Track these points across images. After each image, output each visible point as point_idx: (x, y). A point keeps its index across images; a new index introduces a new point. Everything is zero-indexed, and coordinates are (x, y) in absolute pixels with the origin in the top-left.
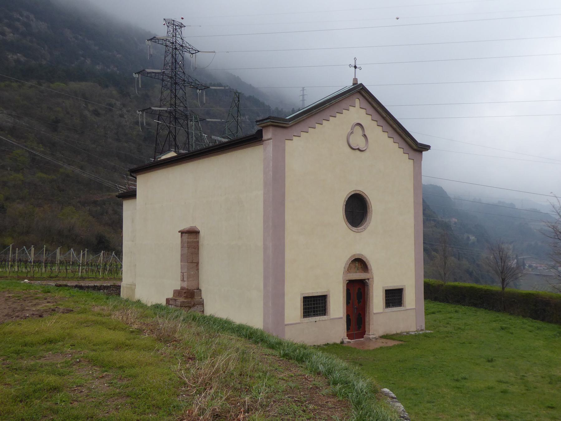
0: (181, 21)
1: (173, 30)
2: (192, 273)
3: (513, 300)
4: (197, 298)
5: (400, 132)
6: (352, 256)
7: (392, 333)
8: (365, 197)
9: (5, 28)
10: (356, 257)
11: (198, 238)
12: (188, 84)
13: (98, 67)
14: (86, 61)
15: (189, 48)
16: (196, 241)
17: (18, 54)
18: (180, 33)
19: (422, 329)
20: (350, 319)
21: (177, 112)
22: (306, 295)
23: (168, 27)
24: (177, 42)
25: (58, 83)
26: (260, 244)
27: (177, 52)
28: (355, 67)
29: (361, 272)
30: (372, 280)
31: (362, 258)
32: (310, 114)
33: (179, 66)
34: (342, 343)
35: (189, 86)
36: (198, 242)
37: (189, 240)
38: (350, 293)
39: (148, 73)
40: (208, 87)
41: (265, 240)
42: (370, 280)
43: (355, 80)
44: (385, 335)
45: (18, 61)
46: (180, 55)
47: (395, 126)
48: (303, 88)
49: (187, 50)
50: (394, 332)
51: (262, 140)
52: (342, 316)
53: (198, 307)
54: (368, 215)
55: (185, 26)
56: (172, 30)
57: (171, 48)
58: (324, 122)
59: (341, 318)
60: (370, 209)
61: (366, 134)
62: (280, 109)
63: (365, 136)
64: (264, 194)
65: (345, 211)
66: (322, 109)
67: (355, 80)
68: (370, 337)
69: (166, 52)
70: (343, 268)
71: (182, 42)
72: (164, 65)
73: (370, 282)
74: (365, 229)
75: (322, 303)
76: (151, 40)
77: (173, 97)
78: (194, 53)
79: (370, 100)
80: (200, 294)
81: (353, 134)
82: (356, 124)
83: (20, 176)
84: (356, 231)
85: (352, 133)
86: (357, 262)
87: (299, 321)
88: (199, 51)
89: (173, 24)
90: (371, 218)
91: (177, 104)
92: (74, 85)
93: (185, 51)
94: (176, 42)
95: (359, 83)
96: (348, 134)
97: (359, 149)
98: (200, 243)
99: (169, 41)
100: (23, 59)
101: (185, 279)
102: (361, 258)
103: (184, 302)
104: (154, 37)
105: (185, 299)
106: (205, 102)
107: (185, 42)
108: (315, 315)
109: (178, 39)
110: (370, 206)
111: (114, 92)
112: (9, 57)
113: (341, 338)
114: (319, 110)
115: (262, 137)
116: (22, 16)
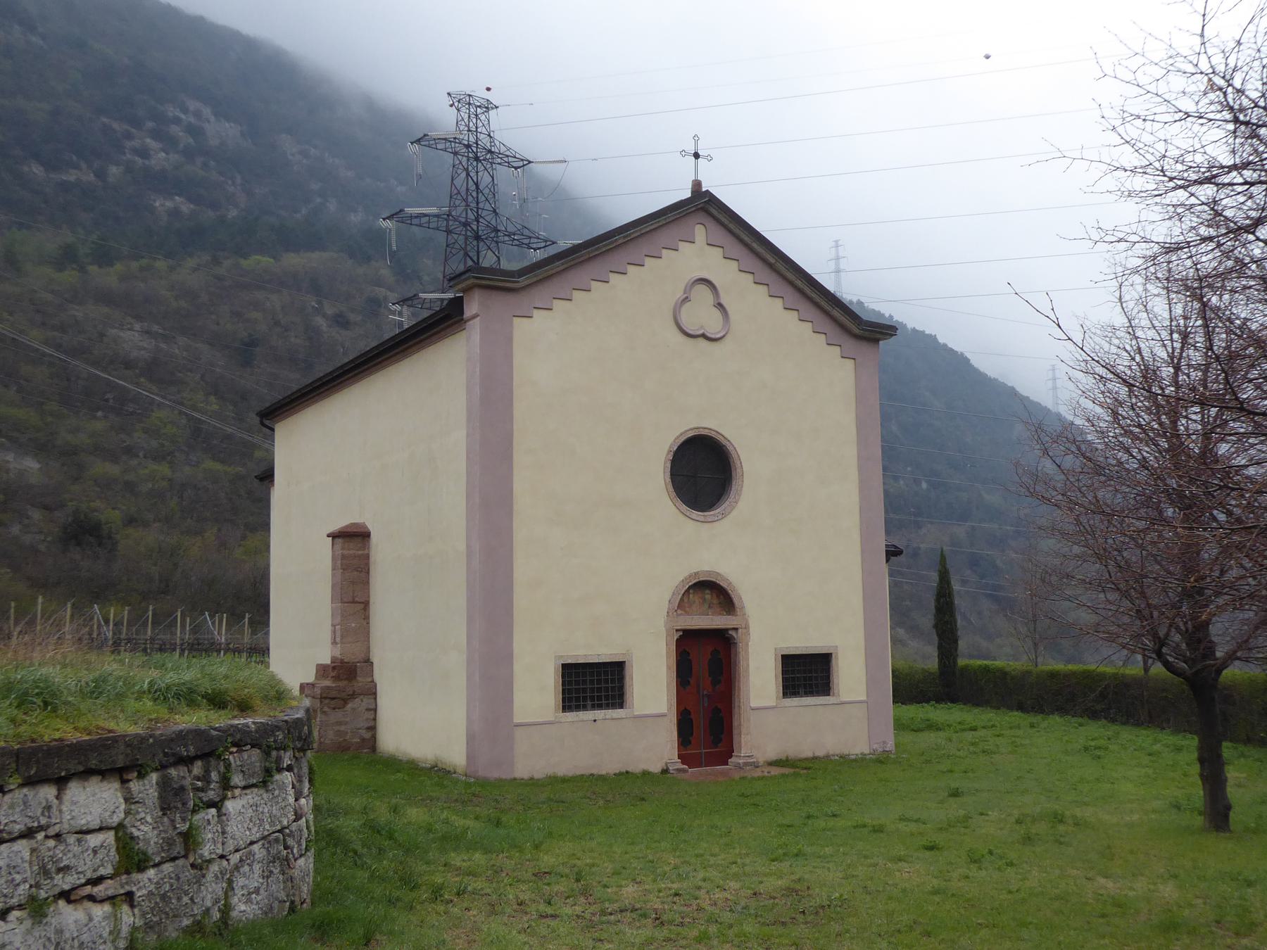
0: (487, 95)
1: (469, 117)
2: (353, 625)
3: (1164, 694)
4: (361, 680)
5: (813, 295)
7: (804, 755)
9: (148, 140)
10: (701, 579)
11: (369, 548)
12: (507, 238)
13: (356, 218)
14: (328, 204)
15: (508, 156)
16: (362, 555)
17: (177, 198)
18: (486, 123)
19: (888, 749)
20: (692, 720)
22: (570, 661)
23: (458, 110)
24: (479, 143)
25: (257, 257)
26: (462, 547)
28: (696, 156)
29: (720, 614)
30: (744, 631)
32: (573, 259)
33: (484, 199)
34: (665, 771)
36: (367, 557)
37: (346, 552)
38: (690, 660)
39: (411, 217)
40: (554, 243)
41: (468, 538)
43: (697, 185)
44: (784, 758)
45: (175, 213)
47: (799, 283)
48: (836, 242)
50: (808, 754)
51: (462, 319)
53: (362, 701)
54: (734, 483)
55: (497, 107)
56: (467, 116)
57: (465, 159)
59: (663, 715)
60: (738, 470)
61: (723, 302)
63: (720, 306)
64: (468, 436)
65: (671, 475)
67: (697, 185)
68: (741, 761)
70: (667, 602)
71: (491, 142)
72: (451, 197)
74: (724, 515)
75: (613, 681)
76: (418, 141)
78: (519, 167)
79: (731, 226)
80: (371, 673)
81: (688, 304)
83: (164, 469)
84: (702, 519)
86: (708, 591)
88: (530, 162)
89: (469, 104)
90: (741, 490)
92: (294, 261)
93: (499, 164)
94: (477, 144)
96: (676, 304)
97: (704, 336)
98: (372, 559)
99: (460, 143)
100: (186, 208)
101: (338, 640)
103: (328, 687)
104: (425, 135)
105: (334, 682)
107: (497, 143)
108: (600, 707)
110: (738, 463)
111: (385, 272)
112: (157, 204)
113: (664, 761)
115: (462, 313)
116: (185, 110)
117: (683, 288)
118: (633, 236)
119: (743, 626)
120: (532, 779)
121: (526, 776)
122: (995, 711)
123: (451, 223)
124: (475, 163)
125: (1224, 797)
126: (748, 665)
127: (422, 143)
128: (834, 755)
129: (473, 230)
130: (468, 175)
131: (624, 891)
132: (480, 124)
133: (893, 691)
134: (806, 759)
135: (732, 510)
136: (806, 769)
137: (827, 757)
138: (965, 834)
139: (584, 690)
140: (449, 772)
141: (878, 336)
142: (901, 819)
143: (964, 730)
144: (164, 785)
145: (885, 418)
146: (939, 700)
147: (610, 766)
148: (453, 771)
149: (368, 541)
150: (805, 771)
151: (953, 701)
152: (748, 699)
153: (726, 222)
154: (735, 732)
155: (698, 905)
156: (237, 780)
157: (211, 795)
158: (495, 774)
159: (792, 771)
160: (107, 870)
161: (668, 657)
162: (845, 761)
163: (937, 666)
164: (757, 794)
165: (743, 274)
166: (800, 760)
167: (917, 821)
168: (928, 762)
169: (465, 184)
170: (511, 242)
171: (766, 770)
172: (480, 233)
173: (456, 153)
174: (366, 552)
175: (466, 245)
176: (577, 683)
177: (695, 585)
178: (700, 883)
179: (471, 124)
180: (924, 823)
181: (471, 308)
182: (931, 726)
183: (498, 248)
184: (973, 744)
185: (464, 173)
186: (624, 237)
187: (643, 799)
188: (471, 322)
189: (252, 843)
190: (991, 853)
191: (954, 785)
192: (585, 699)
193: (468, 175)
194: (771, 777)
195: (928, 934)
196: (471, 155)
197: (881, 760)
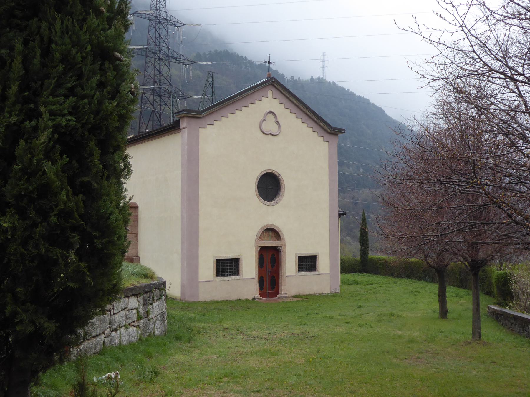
1: (157, 3)
7: (305, 294)
8: (278, 175)
15: (174, 22)
18: (164, 6)
21: (161, 90)
26: (179, 215)
27: (161, 27)
29: (275, 241)
34: (254, 299)
35: (175, 62)
41: (182, 212)
42: (282, 247)
46: (164, 29)
48: (324, 53)
49: (171, 24)
54: (281, 191)
57: (155, 23)
58: (237, 112)
60: (283, 186)
62: (296, 78)
64: (182, 173)
66: (234, 101)
69: (149, 26)
71: (166, 15)
72: (148, 40)
74: (277, 203)
77: (157, 74)
78: (179, 27)
82: (268, 113)
84: (269, 204)
85: (264, 120)
86: (270, 232)
87: (212, 279)
88: (184, 25)
91: (161, 81)
93: (170, 25)
95: (271, 76)
97: (271, 134)
98: (139, 217)
104: (136, 12)
106: (191, 78)
108: (230, 275)
109: (162, 12)
113: (254, 295)
114: (231, 101)
115: (180, 126)
117: (263, 116)
118: (244, 96)
120: (205, 302)
121: (203, 300)
122: (382, 277)
123: (148, 52)
124: (159, 25)
125: (446, 308)
127: (135, 15)
128: (317, 294)
129: (158, 56)
130: (156, 30)
131: (253, 333)
132: (161, 6)
133: (341, 268)
134: (306, 295)
135: (280, 201)
136: (306, 298)
137: (314, 294)
138: (359, 319)
139: (224, 269)
140: (174, 299)
141: (338, 133)
142: (339, 315)
143: (368, 284)
144: (144, 298)
145: (341, 164)
146: (360, 272)
147: (234, 297)
148: (175, 298)
149: (138, 210)
150: (306, 299)
151: (366, 273)
152: (285, 273)
153: (280, 89)
154: (280, 285)
155: (276, 336)
156: (155, 298)
157: (151, 302)
158: (192, 300)
159: (301, 299)
160: (135, 319)
161: (255, 257)
162: (321, 296)
163: (360, 258)
164: (289, 307)
165: (286, 109)
166: (304, 295)
167: (345, 315)
168: (352, 296)
169: (155, 34)
170: (175, 62)
171: (291, 299)
172: (161, 57)
173: (150, 20)
174: (137, 214)
175: (155, 62)
176: (222, 266)
177: (266, 229)
178: (276, 331)
179: (158, 7)
180: (347, 316)
181: (183, 124)
182: (356, 283)
183: (169, 64)
184: (370, 290)
185: (154, 29)
186: (242, 96)
187: (249, 309)
188: (183, 130)
189: (158, 315)
190: (366, 324)
191: (359, 304)
192: (224, 272)
193: (156, 30)
194: (294, 301)
195: (342, 342)
196: (157, 21)
197: (334, 295)
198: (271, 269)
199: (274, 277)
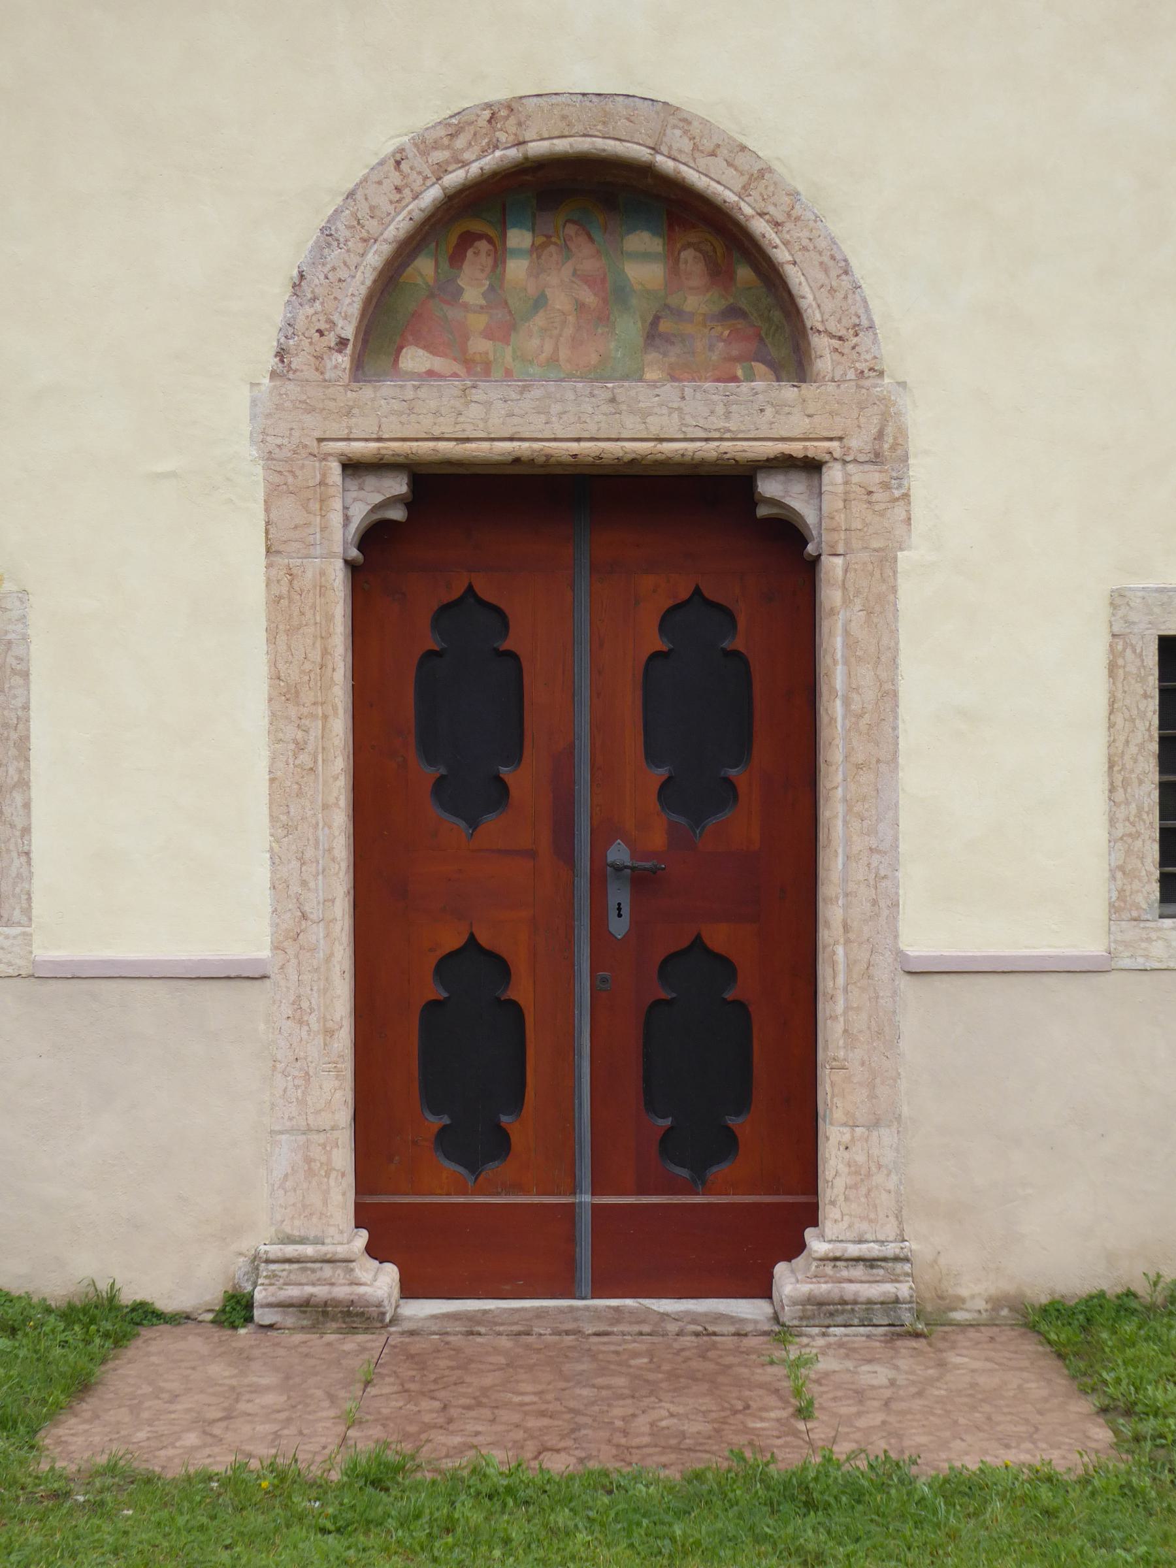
6: (455, 127)
10: (538, 148)
20: (515, 1010)
31: (664, 163)
38: (512, 655)
42: (833, 475)
52: (265, 953)
73: (832, 503)
86: (643, 241)
102: (637, 152)
119: (858, 442)
126: (889, 695)
198: (657, 839)
199: (725, 966)
